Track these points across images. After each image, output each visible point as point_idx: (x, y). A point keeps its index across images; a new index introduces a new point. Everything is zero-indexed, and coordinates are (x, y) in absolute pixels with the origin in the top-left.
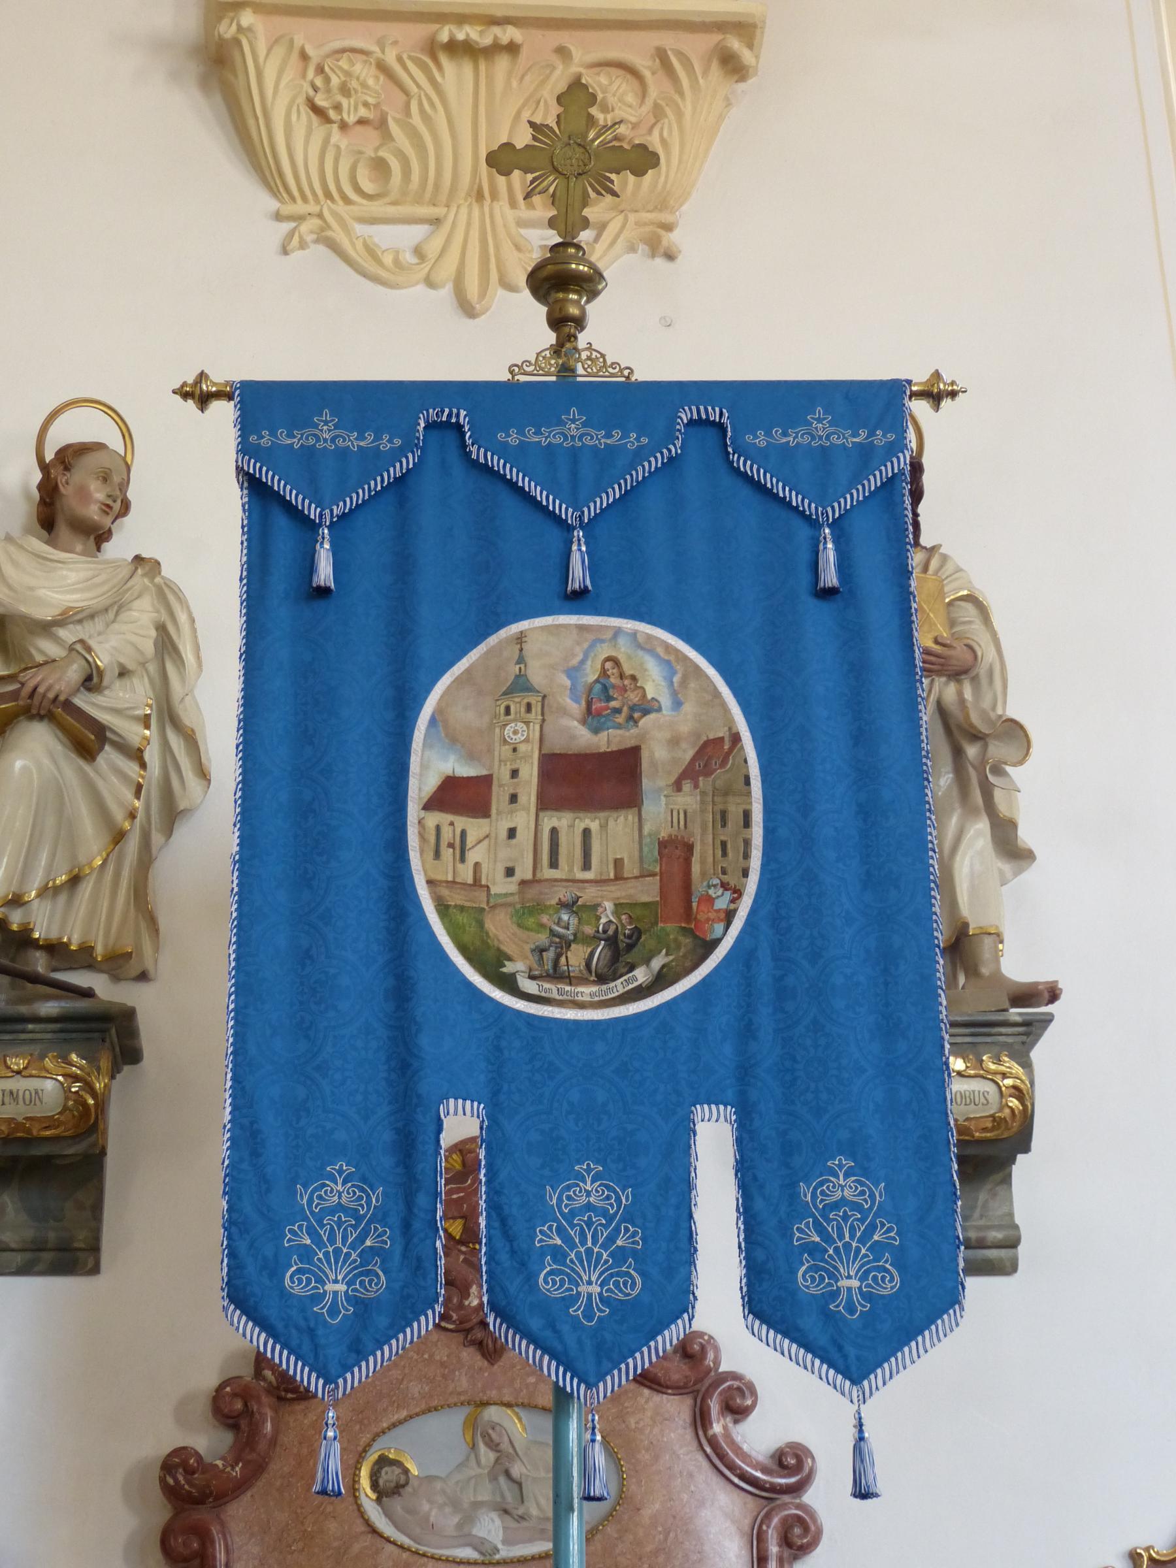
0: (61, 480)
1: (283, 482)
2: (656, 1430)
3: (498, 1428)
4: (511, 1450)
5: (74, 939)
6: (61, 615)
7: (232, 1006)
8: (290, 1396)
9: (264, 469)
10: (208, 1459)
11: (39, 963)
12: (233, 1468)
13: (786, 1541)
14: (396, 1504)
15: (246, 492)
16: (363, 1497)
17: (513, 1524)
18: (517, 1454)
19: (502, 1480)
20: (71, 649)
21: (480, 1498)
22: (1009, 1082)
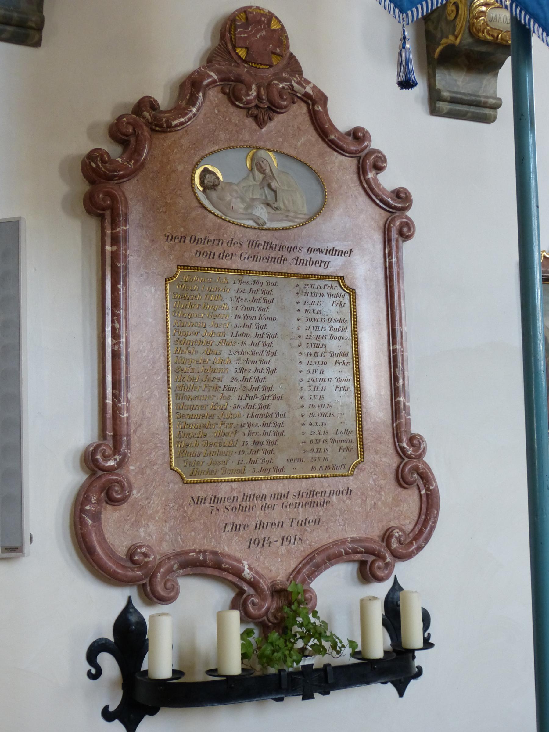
2: (340, 173)
3: (265, 162)
4: (271, 174)
8: (157, 129)
10: (112, 157)
12: (129, 163)
13: (401, 233)
14: (214, 194)
16: (196, 188)
17: (273, 211)
18: (274, 177)
19: (266, 189)
21: (255, 197)
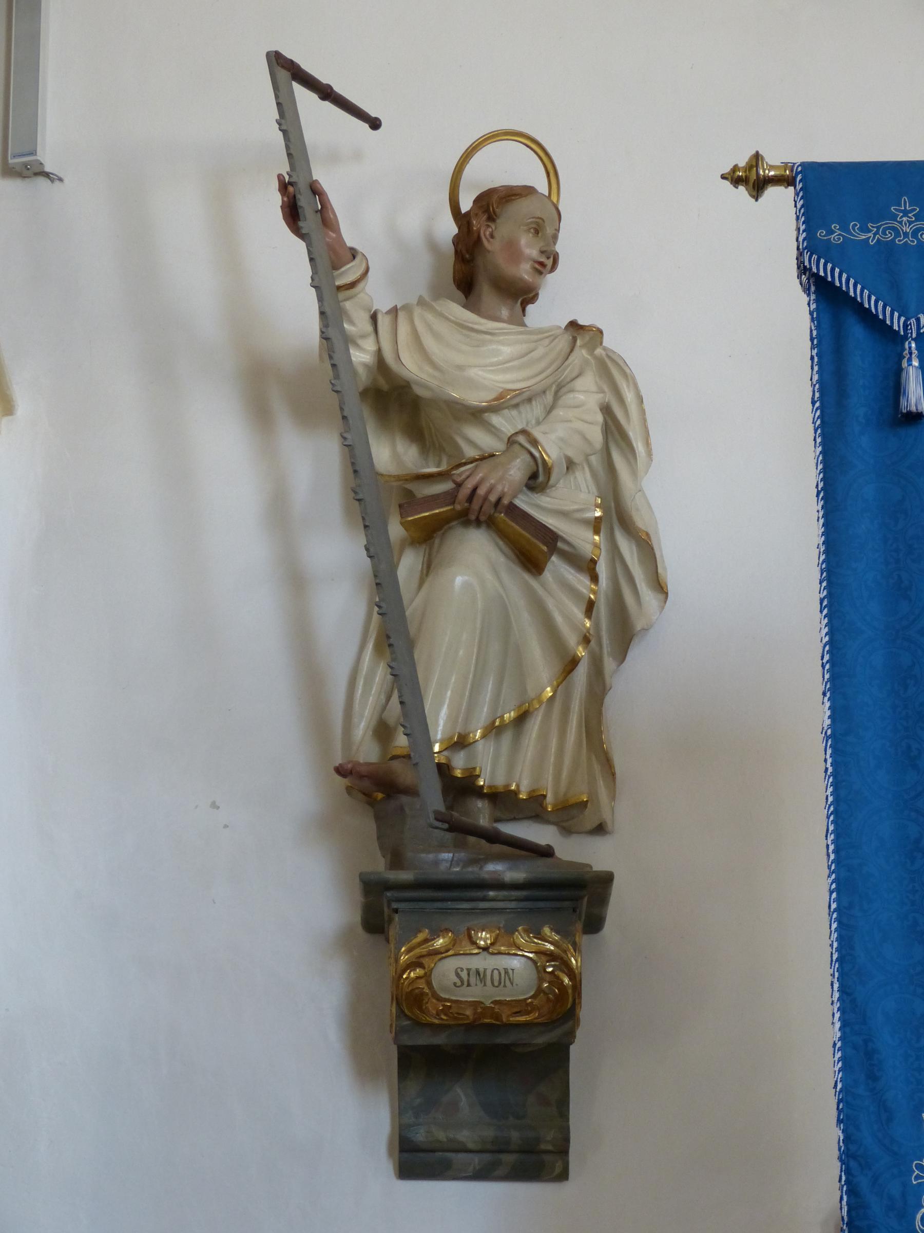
0: (485, 233)
1: (859, 287)
5: (523, 786)
6: (497, 399)
7: (834, 906)
9: (837, 270)
11: (481, 814)
15: (813, 297)
20: (511, 441)
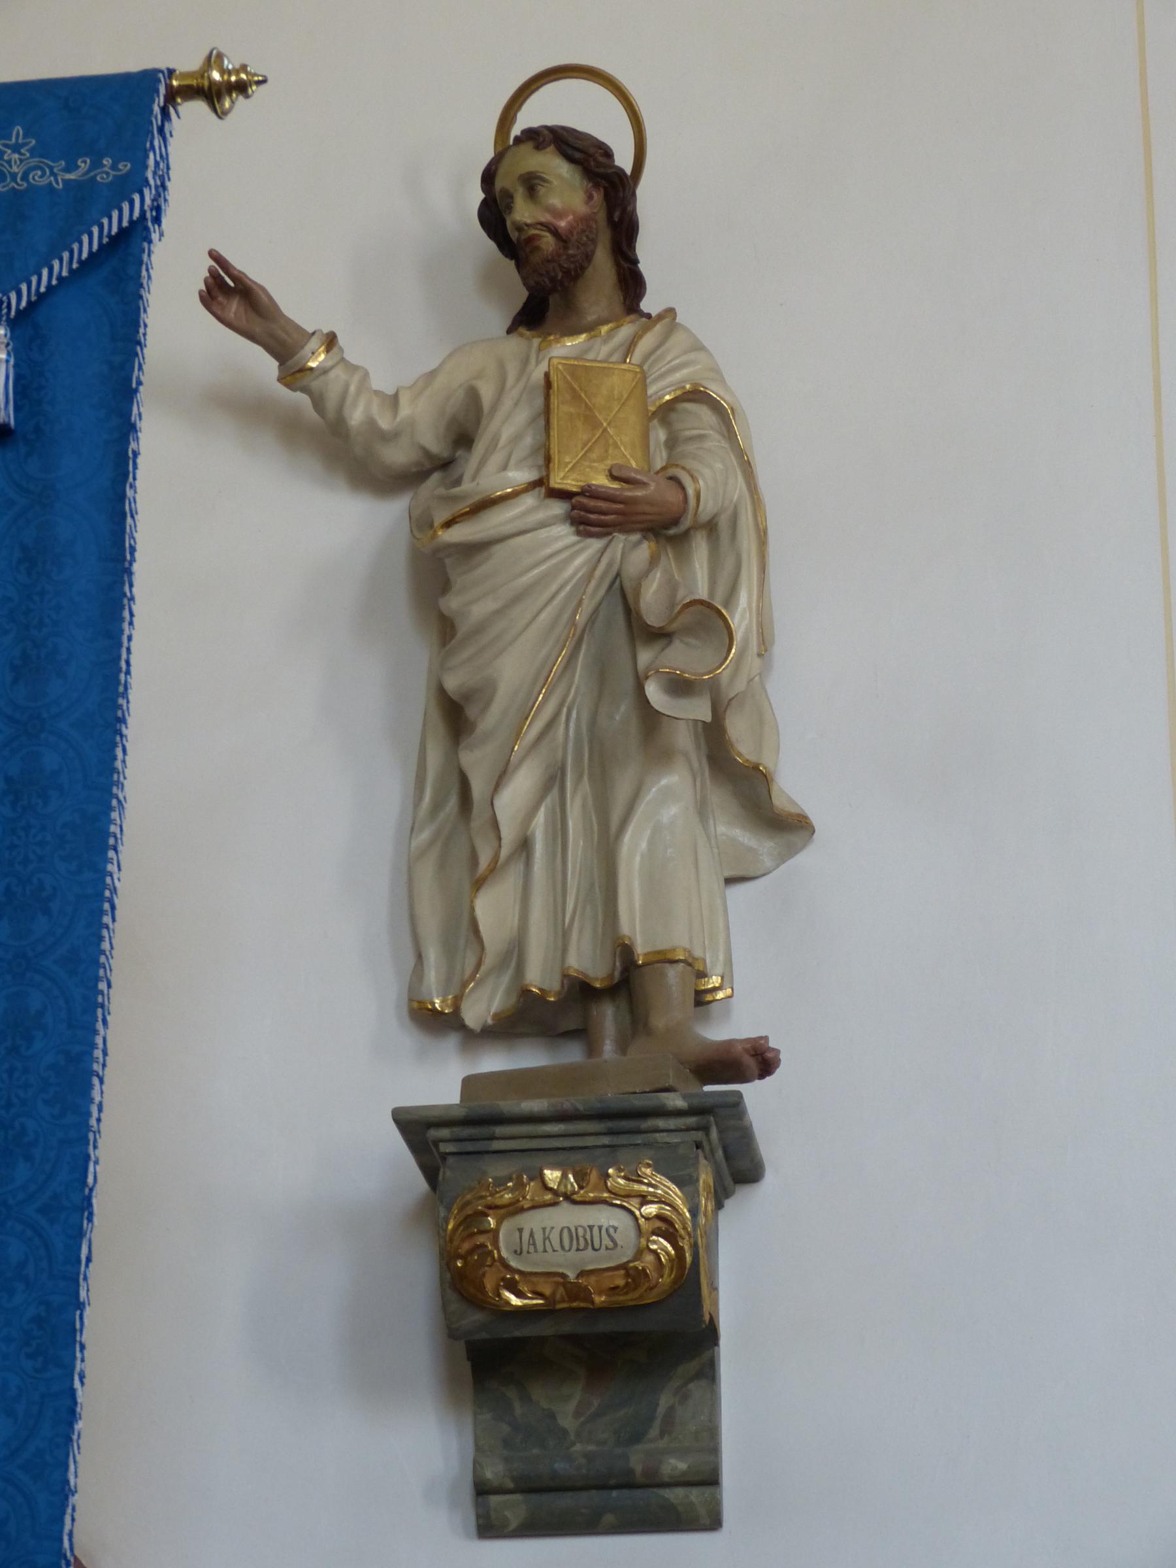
22: (651, 1209)
